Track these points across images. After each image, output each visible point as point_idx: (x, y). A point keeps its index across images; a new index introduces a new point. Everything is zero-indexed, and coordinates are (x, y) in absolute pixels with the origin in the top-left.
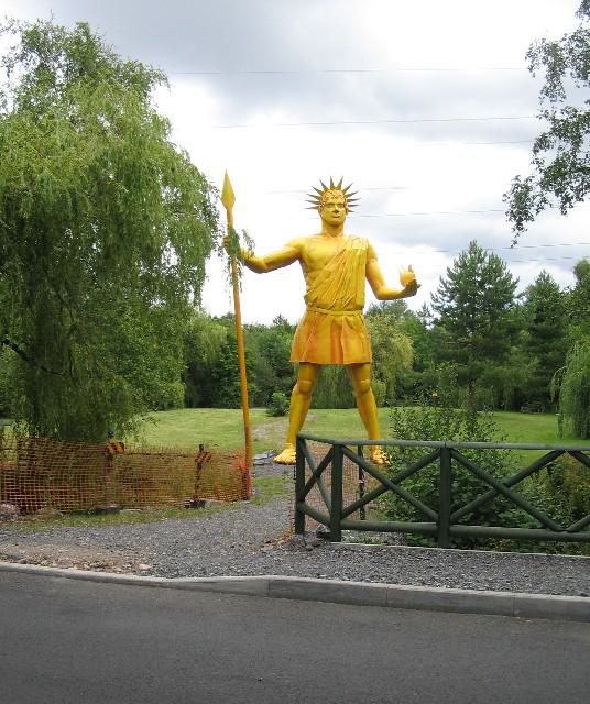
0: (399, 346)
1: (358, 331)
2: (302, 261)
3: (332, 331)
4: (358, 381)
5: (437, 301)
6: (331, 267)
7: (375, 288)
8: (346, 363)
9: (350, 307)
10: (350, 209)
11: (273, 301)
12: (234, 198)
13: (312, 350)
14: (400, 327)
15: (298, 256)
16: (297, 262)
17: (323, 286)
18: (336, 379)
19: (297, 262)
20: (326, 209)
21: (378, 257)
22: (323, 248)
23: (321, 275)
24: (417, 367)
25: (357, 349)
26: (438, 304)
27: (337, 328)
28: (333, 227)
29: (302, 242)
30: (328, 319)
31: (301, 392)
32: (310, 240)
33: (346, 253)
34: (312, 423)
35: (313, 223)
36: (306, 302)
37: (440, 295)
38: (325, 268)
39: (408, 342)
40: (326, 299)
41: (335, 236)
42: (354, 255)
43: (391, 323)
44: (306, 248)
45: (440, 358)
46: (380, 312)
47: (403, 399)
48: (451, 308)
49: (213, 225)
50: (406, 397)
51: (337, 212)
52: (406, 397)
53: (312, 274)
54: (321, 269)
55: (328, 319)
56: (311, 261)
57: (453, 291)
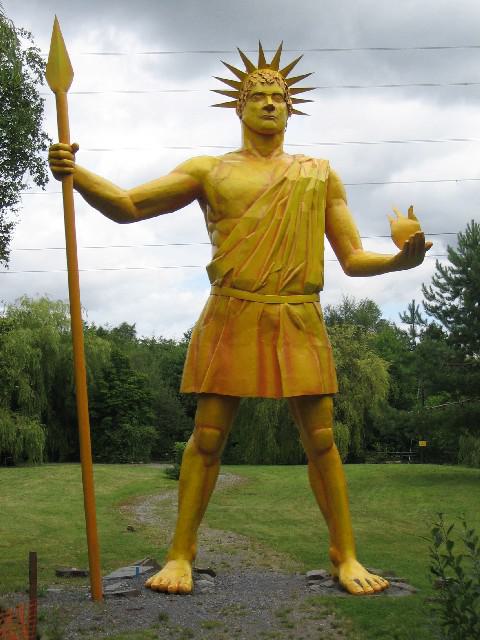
0: (369, 370)
1: (311, 334)
2: (204, 203)
3: (260, 334)
4: (310, 432)
5: (432, 298)
6: (259, 211)
7: (342, 255)
8: (287, 394)
9: (296, 287)
10: (295, 107)
11: (153, 286)
12: (70, 73)
13: (221, 371)
14: (371, 344)
15: (192, 190)
16: (195, 204)
17: (243, 247)
18: (276, 422)
19: (195, 204)
20: (250, 104)
21: (348, 196)
22: (251, 177)
23: (241, 226)
24: (396, 401)
25: (308, 368)
26: (433, 304)
27: (269, 326)
28: (263, 137)
29: (206, 167)
30: (254, 311)
31: (201, 450)
32: (219, 163)
33: (287, 187)
34: (234, 491)
35: (225, 133)
36: (212, 279)
37: (436, 289)
38: (248, 214)
39: (382, 366)
40: (249, 271)
41: (267, 155)
42: (302, 193)
43: (357, 336)
44: (212, 174)
45: (438, 387)
46: (340, 321)
47: (374, 449)
48: (454, 308)
49: (33, 128)
50: (378, 446)
51: (270, 108)
52: (378, 446)
53: (223, 225)
54: (240, 216)
55: (254, 311)
56: (221, 199)
57: (456, 283)
